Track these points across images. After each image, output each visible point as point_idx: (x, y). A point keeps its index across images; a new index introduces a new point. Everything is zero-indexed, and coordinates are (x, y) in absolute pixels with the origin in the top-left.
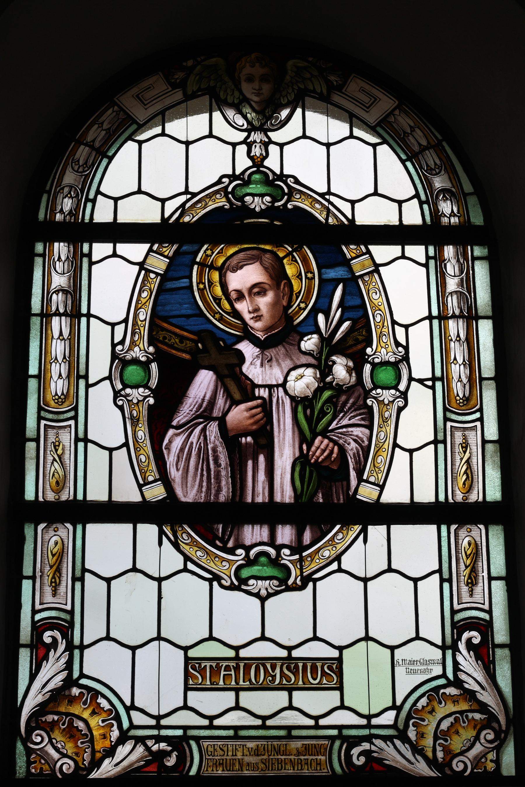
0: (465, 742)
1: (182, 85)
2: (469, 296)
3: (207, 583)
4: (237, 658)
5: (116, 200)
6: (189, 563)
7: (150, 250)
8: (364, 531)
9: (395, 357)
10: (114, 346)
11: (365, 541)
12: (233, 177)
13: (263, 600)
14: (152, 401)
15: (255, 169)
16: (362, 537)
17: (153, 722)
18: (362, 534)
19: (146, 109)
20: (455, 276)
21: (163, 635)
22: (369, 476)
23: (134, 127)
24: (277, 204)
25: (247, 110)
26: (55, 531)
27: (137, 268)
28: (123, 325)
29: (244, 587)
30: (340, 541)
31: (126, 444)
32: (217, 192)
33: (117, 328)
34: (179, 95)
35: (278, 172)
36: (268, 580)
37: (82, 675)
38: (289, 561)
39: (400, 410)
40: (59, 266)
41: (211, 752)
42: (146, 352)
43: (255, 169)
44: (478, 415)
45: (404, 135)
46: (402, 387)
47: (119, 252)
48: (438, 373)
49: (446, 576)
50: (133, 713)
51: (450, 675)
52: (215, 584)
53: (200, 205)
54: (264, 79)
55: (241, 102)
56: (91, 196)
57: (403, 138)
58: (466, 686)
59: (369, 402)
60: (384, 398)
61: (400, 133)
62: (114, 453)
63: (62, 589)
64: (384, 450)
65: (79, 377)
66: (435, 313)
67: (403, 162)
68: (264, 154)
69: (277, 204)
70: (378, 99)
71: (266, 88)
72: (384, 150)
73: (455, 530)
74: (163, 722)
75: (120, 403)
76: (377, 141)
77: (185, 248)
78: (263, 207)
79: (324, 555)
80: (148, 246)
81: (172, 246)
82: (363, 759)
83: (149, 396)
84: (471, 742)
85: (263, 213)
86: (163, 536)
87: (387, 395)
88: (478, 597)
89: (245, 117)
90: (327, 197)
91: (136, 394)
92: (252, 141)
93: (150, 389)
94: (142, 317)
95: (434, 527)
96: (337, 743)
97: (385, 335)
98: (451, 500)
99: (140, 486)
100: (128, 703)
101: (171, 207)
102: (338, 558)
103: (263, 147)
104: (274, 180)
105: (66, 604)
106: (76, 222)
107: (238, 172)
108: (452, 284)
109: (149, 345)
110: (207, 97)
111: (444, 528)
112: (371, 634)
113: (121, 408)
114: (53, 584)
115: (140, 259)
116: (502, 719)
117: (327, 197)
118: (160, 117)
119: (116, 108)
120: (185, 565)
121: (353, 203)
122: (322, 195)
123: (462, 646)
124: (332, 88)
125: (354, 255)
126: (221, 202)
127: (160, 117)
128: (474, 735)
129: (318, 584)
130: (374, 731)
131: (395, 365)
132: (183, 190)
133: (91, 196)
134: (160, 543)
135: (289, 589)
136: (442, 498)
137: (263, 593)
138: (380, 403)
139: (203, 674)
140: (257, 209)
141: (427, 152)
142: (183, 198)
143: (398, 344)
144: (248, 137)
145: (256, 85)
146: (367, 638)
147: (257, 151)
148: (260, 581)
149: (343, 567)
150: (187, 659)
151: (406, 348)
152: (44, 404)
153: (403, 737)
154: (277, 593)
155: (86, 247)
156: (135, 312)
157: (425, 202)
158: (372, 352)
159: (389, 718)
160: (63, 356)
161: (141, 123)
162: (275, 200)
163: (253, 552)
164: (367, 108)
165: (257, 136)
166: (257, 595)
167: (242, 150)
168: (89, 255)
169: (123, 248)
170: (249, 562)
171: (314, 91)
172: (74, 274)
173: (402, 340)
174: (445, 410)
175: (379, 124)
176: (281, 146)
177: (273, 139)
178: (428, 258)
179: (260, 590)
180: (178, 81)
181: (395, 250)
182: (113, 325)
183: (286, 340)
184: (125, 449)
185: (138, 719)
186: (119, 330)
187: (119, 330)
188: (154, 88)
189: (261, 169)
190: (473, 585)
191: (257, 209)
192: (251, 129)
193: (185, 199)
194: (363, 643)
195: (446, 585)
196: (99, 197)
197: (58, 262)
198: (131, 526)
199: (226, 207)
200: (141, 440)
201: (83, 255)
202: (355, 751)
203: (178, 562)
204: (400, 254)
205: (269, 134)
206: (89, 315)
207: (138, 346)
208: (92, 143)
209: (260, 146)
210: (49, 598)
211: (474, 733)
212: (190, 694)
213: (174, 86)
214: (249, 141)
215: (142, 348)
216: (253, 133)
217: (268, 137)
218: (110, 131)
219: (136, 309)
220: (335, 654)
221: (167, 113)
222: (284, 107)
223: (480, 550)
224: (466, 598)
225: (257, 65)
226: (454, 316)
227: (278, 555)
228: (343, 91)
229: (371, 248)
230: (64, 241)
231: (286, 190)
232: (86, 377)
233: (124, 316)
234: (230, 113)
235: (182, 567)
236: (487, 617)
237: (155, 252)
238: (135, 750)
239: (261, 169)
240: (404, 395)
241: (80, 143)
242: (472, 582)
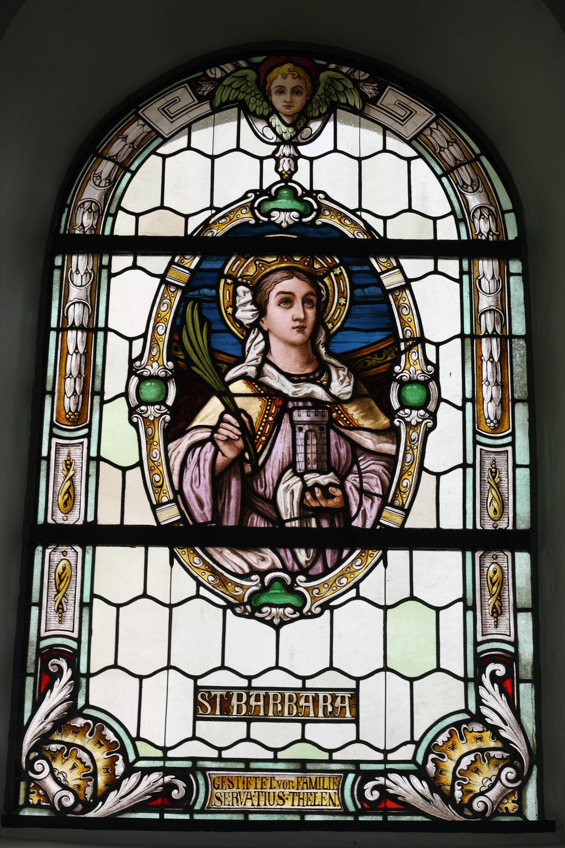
0: (485, 780)
1: (211, 97)
2: (502, 314)
3: (221, 611)
4: (250, 687)
5: (138, 216)
7: (171, 263)
9: (424, 376)
10: (131, 361)
11: (385, 565)
12: (258, 193)
13: (277, 628)
14: (168, 418)
15: (283, 184)
16: (381, 563)
17: (159, 754)
18: (382, 561)
19: (172, 122)
22: (411, 312)
24: (304, 220)
25: (275, 121)
26: (64, 556)
27: (158, 280)
28: (141, 340)
29: (257, 615)
30: (361, 567)
31: (140, 464)
32: (243, 206)
33: (135, 343)
34: (206, 108)
35: (308, 188)
37: (87, 705)
38: (305, 588)
40: (77, 279)
41: (218, 785)
42: (165, 368)
43: (283, 184)
44: (509, 439)
46: (431, 407)
47: (139, 264)
49: (470, 603)
50: (138, 743)
51: (472, 707)
52: (229, 612)
53: (224, 220)
54: (295, 91)
55: (270, 115)
56: (112, 211)
57: (439, 153)
58: (488, 721)
59: (396, 422)
61: (436, 149)
63: (69, 615)
64: (410, 473)
65: (94, 393)
66: (467, 331)
67: (439, 177)
68: (293, 170)
69: (304, 220)
70: (414, 112)
71: (299, 101)
72: (419, 165)
73: (480, 557)
74: (170, 754)
75: (135, 420)
77: (207, 265)
78: (291, 222)
79: (342, 583)
80: (168, 259)
81: (194, 258)
82: (376, 794)
83: (166, 413)
84: (491, 781)
85: (290, 228)
87: (414, 416)
88: (503, 628)
90: (358, 213)
91: (152, 411)
92: (282, 155)
94: (161, 330)
95: (459, 554)
96: (351, 777)
98: (478, 527)
99: (154, 508)
100: (134, 735)
101: (194, 223)
102: (356, 586)
103: (291, 161)
104: (303, 196)
105: (73, 632)
106: (96, 236)
107: (265, 187)
108: (485, 302)
110: (236, 109)
111: (469, 554)
112: (389, 665)
114: (60, 610)
115: (161, 271)
116: (525, 760)
117: (358, 213)
118: (186, 130)
119: (141, 122)
121: (385, 219)
122: (353, 212)
123: (486, 680)
124: (366, 100)
125: (384, 269)
126: (245, 216)
127: (186, 130)
128: (496, 775)
129: (336, 611)
130: (389, 766)
131: (425, 384)
132: (208, 205)
133: (112, 211)
134: (172, 564)
135: (303, 617)
136: (469, 526)
137: (276, 621)
138: (408, 424)
140: (284, 225)
141: (463, 167)
142: (208, 213)
143: (427, 362)
144: (276, 151)
145: (287, 97)
146: (386, 669)
147: (285, 165)
148: (275, 609)
149: (362, 594)
150: (197, 689)
151: (436, 366)
152: (56, 421)
153: (421, 773)
154: (293, 620)
155: (105, 261)
156: (155, 324)
159: (406, 753)
160: (75, 347)
161: (167, 137)
162: (302, 215)
164: (403, 121)
165: (286, 150)
166: (270, 623)
167: (270, 164)
168: (109, 267)
169: (143, 261)
170: (264, 589)
171: (347, 104)
172: (91, 288)
173: (432, 358)
174: (475, 433)
175: (415, 138)
176: (311, 160)
177: (302, 153)
178: (462, 273)
179: (274, 617)
180: (206, 93)
181: (427, 264)
182: (131, 340)
183: (305, 479)
184: (138, 469)
185: (144, 750)
186: (138, 345)
187: (138, 345)
188: (180, 100)
189: (290, 184)
190: (498, 615)
191: (284, 225)
192: (281, 142)
193: (210, 214)
194: (389, 603)
195: (470, 614)
196: (120, 212)
197: (75, 274)
199: (250, 222)
200: (156, 458)
201: (102, 267)
202: (369, 785)
203: (190, 588)
204: (432, 269)
205: (300, 148)
206: (106, 329)
207: (157, 361)
208: (115, 158)
209: (289, 161)
210: (54, 623)
211: (496, 772)
212: (198, 723)
213: (201, 99)
214: (277, 155)
215: (161, 363)
216: (282, 146)
217: (297, 151)
219: (156, 322)
220: (352, 684)
221: (193, 125)
222: (315, 119)
223: (507, 581)
224: (491, 629)
225: (289, 77)
228: (378, 104)
229: (403, 262)
230: (82, 254)
231: (315, 206)
232: (102, 393)
233: (142, 331)
234: (260, 126)
236: (511, 649)
238: (109, 173)
239: (290, 184)
240: (433, 416)
241: (103, 157)
242: (497, 612)
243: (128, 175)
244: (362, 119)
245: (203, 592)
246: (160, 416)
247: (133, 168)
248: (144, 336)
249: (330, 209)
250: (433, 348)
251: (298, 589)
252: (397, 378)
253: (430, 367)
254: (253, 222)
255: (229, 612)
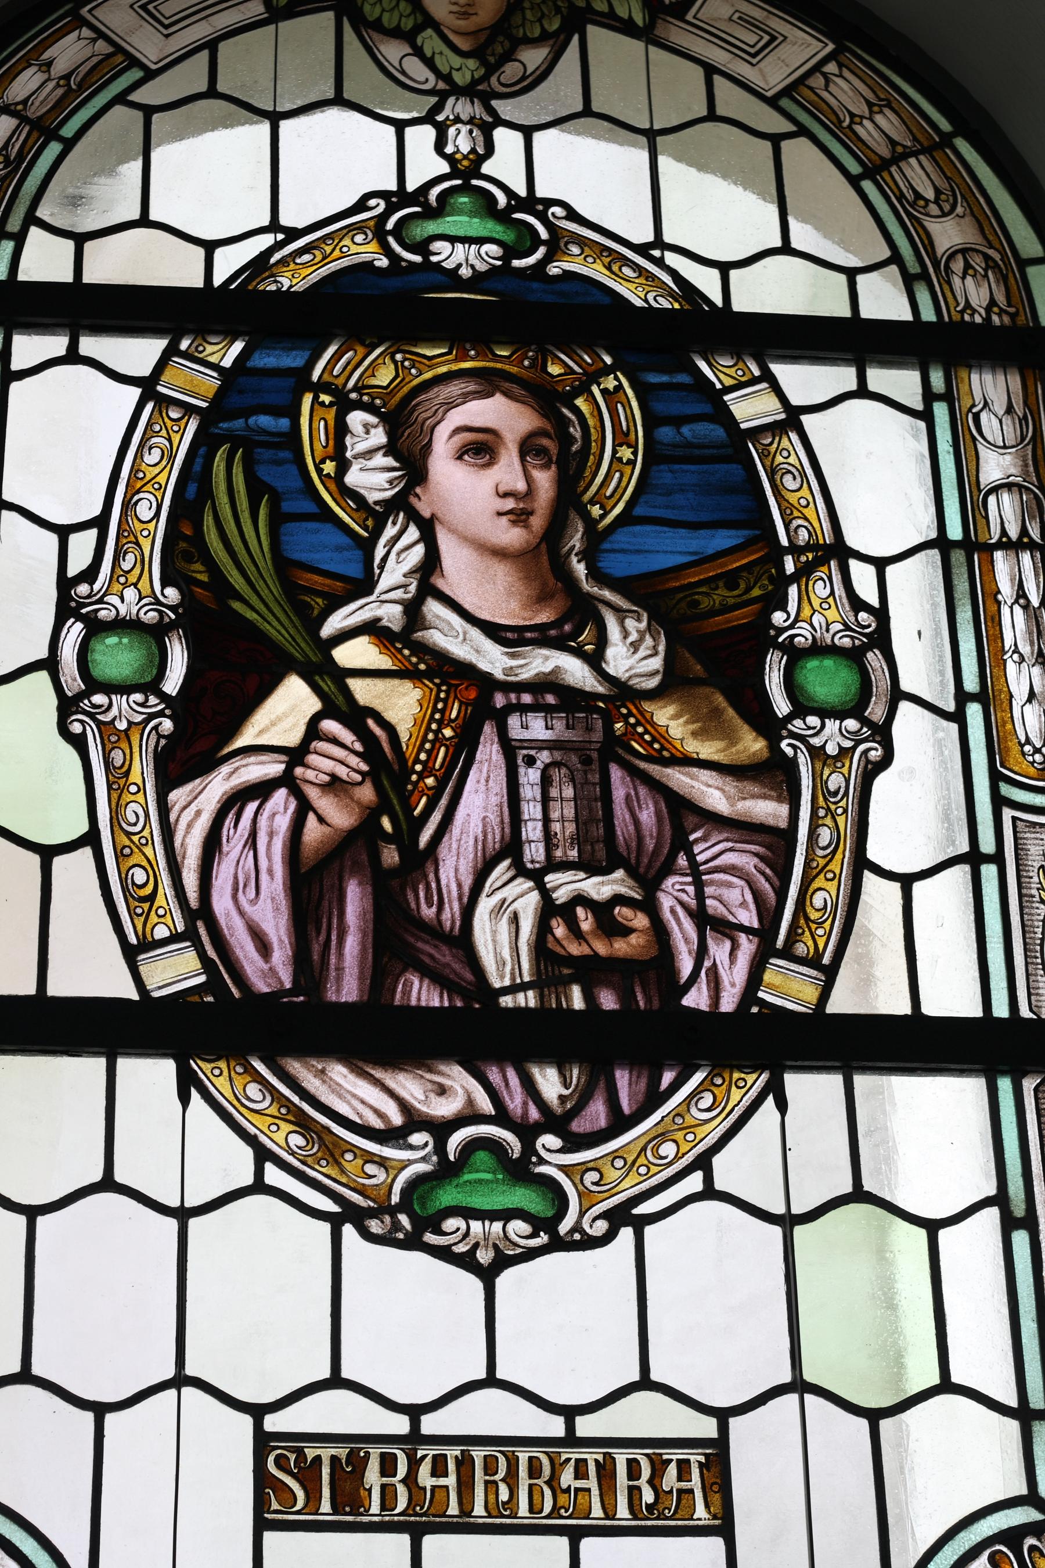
4: (415, 1438)
6: (270, 1168)
8: (776, 1090)
9: (852, 638)
10: (65, 584)
11: (782, 1106)
13: (488, 1276)
14: (167, 725)
20: (1005, 447)
21: (172, 1225)
23: (136, 74)
24: (516, 263)
27: (134, 393)
28: (93, 534)
29: (430, 1238)
31: (91, 839)
33: (74, 539)
35: (522, 191)
36: (498, 1219)
38: (562, 1168)
39: (872, 771)
42: (158, 602)
45: (852, 122)
46: (876, 711)
48: (971, 684)
53: (307, 257)
55: (418, 29)
57: (850, 127)
60: (826, 741)
61: (842, 118)
62: (59, 863)
64: (830, 875)
67: (854, 182)
69: (516, 263)
73: (1036, 1090)
75: (76, 728)
76: (785, 126)
77: (264, 360)
80: (159, 345)
83: (161, 714)
85: (479, 282)
86: (193, 1091)
89: (429, 63)
90: (656, 253)
92: (451, 117)
93: (163, 697)
97: (822, 579)
99: (131, 954)
102: (703, 1163)
104: (510, 209)
107: (411, 186)
109: (164, 585)
111: (1005, 1085)
113: (79, 743)
115: (144, 370)
117: (656, 253)
120: (259, 1172)
121: (724, 268)
122: (642, 249)
125: (728, 382)
129: (650, 1232)
132: (265, 221)
138: (817, 753)
139: (309, 1486)
142: (267, 240)
143: (857, 604)
150: (263, 1441)
151: (882, 614)
154: (531, 1254)
157: (917, 277)
158: (785, 621)
161: (154, 67)
162: (510, 252)
163: (456, 1140)
164: (753, 56)
166: (466, 1262)
167: (422, 137)
174: (996, 778)
175: (787, 92)
178: (929, 396)
182: (63, 532)
184: (87, 852)
189: (474, 182)
196: (34, 232)
198: (100, 1064)
200: (135, 824)
207: (135, 585)
208: (20, 107)
209: (471, 132)
216: (451, 101)
217: (492, 112)
218: (69, 81)
226: (1006, 544)
227: (528, 1148)
228: (689, 17)
231: (544, 234)
234: (393, 51)
235: (248, 1179)
237: (186, 355)
240: (883, 733)
243: (54, 149)
244: (651, 48)
245: (273, 1175)
246: (146, 721)
247: (68, 131)
248: (100, 523)
249: (582, 242)
250: (870, 570)
251: (543, 1169)
252: (780, 640)
253: (863, 616)
254: (383, 262)
255: (349, 1231)
